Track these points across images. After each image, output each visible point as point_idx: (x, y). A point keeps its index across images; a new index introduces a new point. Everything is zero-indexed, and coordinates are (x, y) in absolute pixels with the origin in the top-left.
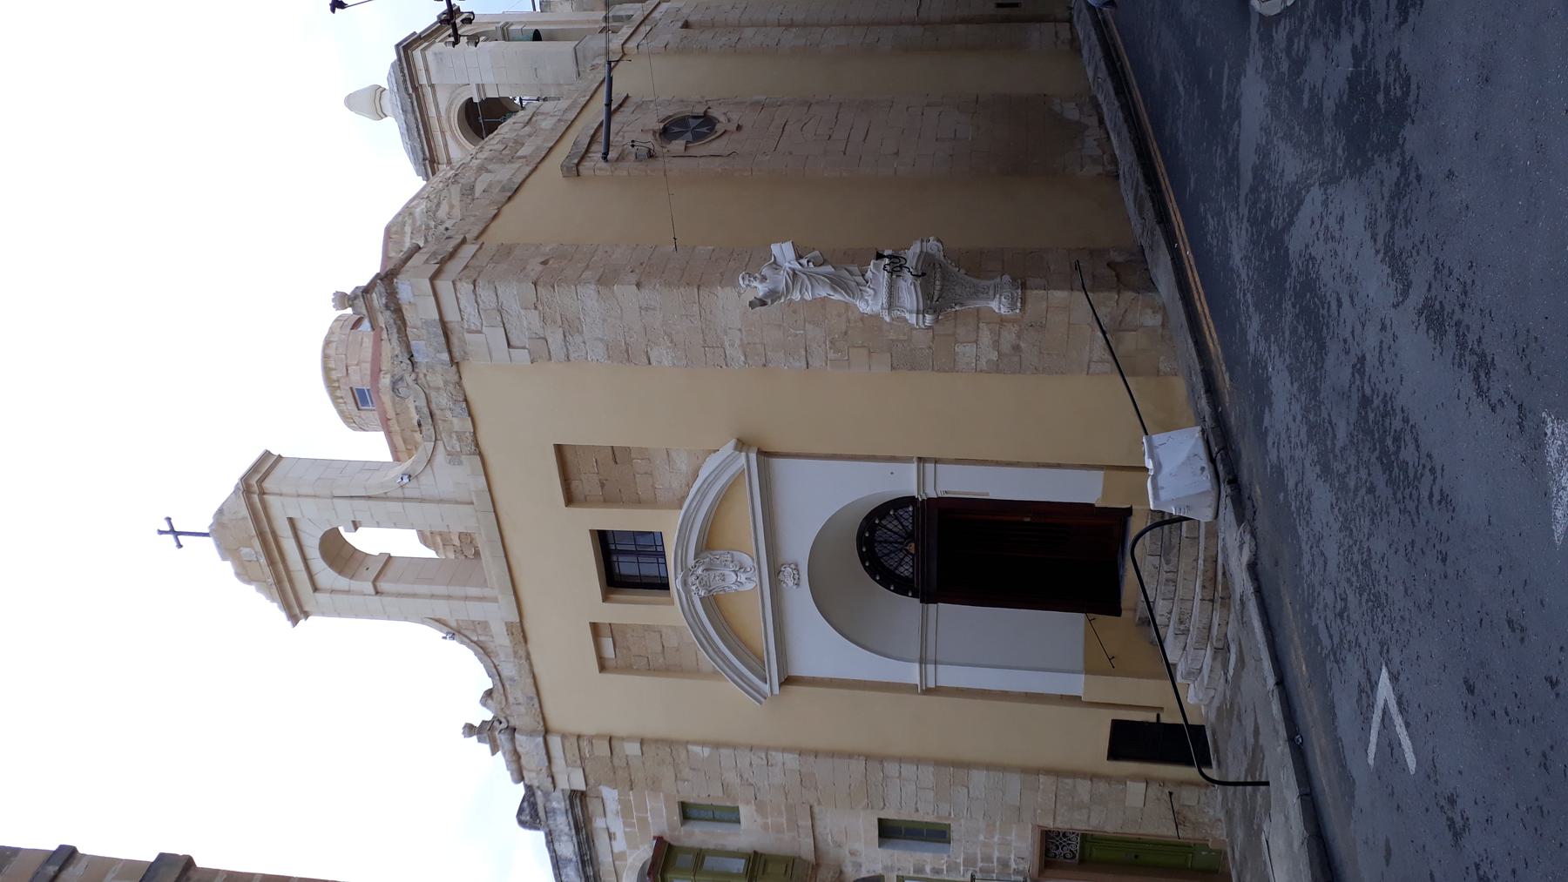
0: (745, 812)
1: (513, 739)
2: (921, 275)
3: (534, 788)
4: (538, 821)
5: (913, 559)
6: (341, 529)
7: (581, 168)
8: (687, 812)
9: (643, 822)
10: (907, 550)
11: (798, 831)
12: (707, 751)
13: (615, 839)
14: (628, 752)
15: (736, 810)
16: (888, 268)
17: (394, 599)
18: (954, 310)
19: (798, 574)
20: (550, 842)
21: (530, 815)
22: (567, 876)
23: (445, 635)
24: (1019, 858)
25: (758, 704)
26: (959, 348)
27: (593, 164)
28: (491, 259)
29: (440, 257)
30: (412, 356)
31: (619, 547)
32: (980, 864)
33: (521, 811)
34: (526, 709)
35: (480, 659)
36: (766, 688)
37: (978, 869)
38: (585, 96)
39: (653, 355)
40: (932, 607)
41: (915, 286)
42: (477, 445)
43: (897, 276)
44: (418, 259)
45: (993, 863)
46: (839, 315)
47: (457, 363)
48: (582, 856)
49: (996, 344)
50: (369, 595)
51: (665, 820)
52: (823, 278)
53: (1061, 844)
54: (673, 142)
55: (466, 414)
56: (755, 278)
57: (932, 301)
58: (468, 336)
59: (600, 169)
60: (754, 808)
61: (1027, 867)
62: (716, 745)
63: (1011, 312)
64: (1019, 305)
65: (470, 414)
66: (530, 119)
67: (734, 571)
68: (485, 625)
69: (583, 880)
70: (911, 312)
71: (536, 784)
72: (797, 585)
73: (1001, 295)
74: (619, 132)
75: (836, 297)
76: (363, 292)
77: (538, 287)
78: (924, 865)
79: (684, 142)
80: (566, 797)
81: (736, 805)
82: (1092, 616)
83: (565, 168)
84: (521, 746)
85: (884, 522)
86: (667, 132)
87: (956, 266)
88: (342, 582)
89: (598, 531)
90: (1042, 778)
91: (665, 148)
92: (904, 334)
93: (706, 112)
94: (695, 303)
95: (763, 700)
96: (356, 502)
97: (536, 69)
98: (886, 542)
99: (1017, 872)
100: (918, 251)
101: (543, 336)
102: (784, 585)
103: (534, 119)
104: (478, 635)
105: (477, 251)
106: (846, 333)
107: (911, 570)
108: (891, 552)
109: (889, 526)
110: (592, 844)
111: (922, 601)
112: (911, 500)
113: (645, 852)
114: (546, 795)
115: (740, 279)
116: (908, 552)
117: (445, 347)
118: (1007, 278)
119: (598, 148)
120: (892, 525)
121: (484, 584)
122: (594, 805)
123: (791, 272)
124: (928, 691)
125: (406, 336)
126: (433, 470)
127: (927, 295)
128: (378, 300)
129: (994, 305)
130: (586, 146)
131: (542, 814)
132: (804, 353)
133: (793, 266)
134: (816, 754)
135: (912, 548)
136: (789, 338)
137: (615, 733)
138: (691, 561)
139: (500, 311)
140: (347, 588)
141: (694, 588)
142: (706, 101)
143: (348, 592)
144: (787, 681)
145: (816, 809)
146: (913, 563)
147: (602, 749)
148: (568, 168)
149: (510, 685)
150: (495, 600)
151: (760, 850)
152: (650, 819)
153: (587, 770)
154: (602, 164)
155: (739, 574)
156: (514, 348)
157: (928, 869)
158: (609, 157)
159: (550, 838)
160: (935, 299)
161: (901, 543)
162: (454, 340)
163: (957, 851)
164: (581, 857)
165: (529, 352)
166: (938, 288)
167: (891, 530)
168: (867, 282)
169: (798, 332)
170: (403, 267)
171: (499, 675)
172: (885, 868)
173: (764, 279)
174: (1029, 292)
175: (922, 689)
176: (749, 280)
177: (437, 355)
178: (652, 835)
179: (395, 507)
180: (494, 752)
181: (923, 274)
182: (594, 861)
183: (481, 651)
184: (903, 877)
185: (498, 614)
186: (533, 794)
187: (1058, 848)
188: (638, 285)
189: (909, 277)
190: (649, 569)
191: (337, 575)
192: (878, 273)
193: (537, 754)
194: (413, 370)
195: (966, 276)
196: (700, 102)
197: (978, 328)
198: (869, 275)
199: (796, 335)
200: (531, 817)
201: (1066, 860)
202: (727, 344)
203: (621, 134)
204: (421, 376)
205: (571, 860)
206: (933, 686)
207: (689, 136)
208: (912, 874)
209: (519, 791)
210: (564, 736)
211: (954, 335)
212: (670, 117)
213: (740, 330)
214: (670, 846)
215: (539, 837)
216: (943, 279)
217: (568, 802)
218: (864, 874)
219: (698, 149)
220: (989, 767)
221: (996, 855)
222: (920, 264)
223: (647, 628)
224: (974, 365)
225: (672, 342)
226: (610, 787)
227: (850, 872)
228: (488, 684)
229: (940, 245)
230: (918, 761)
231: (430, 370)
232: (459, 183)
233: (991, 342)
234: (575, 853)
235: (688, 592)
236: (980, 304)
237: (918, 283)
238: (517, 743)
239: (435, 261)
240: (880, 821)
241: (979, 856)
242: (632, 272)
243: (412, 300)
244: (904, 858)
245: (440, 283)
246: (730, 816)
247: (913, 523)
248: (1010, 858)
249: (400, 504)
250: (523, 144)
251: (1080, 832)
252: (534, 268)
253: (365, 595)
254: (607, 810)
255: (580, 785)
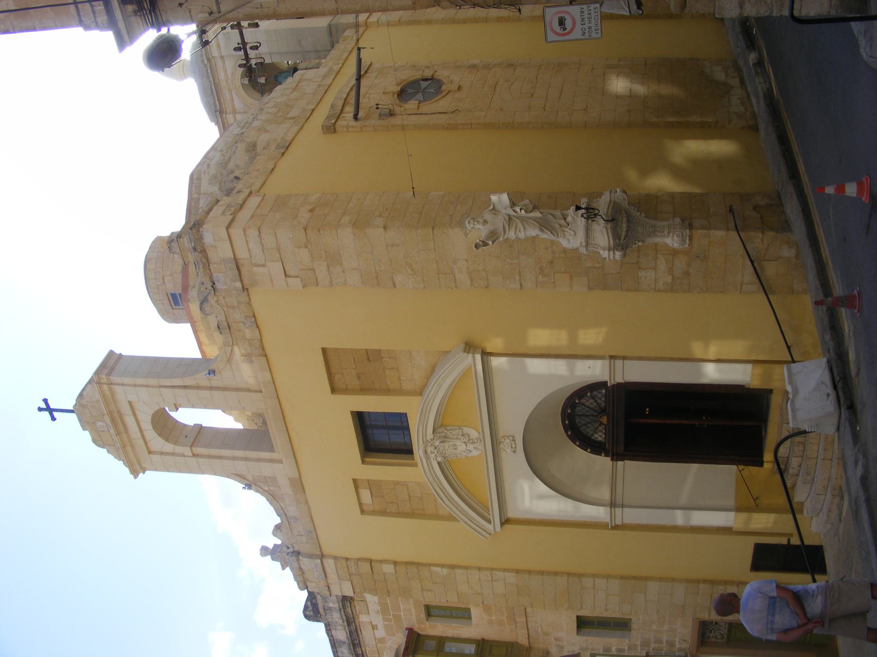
0: (474, 612)
1: (298, 560)
2: (612, 220)
3: (315, 593)
4: (319, 615)
5: (605, 428)
6: (167, 408)
7: (337, 126)
8: (430, 611)
9: (397, 618)
10: (600, 422)
11: (516, 625)
12: (445, 571)
13: (377, 629)
14: (385, 571)
15: (468, 610)
16: (585, 215)
17: (206, 460)
18: (637, 245)
19: (515, 444)
20: (329, 630)
21: (312, 611)
22: (342, 653)
23: (244, 486)
24: (682, 640)
25: (485, 539)
26: (642, 274)
27: (346, 122)
28: (271, 209)
29: (233, 209)
30: (214, 284)
31: (373, 423)
32: (653, 645)
33: (306, 608)
34: (307, 539)
35: (271, 503)
36: (490, 527)
37: (651, 649)
38: (338, 64)
39: (398, 279)
40: (620, 464)
41: (606, 229)
42: (263, 349)
43: (592, 221)
44: (217, 210)
45: (663, 644)
46: (546, 248)
47: (247, 289)
48: (352, 641)
49: (670, 271)
50: (188, 456)
51: (414, 617)
52: (532, 221)
53: (713, 629)
54: (409, 102)
55: (255, 326)
56: (478, 222)
57: (620, 240)
58: (256, 269)
59: (353, 127)
60: (482, 609)
61: (688, 646)
62: (453, 567)
63: (681, 247)
64: (688, 241)
65: (257, 327)
66: (297, 85)
67: (465, 442)
68: (274, 479)
69: (354, 655)
70: (604, 249)
71: (316, 591)
72: (514, 452)
73: (673, 234)
74: (366, 94)
75: (544, 236)
76: (177, 238)
77: (307, 231)
78: (611, 647)
79: (417, 102)
80: (340, 600)
81: (469, 607)
82: (741, 467)
83: (325, 128)
84: (304, 565)
85: (583, 401)
86: (403, 94)
87: (638, 211)
88: (169, 447)
89: (357, 412)
90: (702, 586)
91: (403, 107)
92: (599, 263)
93: (433, 75)
94: (430, 241)
95: (488, 536)
96: (176, 391)
97: (300, 41)
98: (584, 415)
99: (680, 649)
100: (608, 199)
101: (311, 267)
102: (504, 452)
103: (300, 84)
104: (268, 486)
105: (261, 202)
106: (552, 262)
107: (604, 436)
108: (589, 423)
109: (587, 404)
110: (359, 632)
111: (612, 460)
112: (603, 385)
113: (399, 639)
114: (325, 599)
115: (467, 223)
116: (601, 424)
117: (238, 277)
118: (678, 220)
119: (350, 109)
120: (589, 402)
121: (272, 450)
122: (358, 607)
123: (507, 218)
124: (616, 527)
125: (210, 270)
126: (231, 366)
127: (616, 236)
128: (186, 243)
129: (668, 241)
130: (340, 108)
131: (321, 611)
132: (518, 278)
133: (508, 213)
134: (530, 572)
135: (604, 420)
136: (506, 266)
137: (373, 558)
138: (430, 435)
139: (279, 250)
140: (172, 451)
141: (433, 455)
142: (433, 66)
143: (173, 454)
144: (505, 521)
145: (529, 610)
146: (606, 431)
147: (365, 568)
148: (327, 126)
149: (294, 522)
150: (280, 462)
151: (486, 638)
152: (403, 616)
153: (354, 583)
154: (353, 123)
155: (468, 444)
156: (290, 277)
157: (614, 649)
158: (359, 116)
159: (328, 628)
160: (623, 238)
161: (596, 416)
162: (244, 271)
163: (636, 636)
164: (352, 641)
165: (302, 280)
166: (625, 229)
167: (588, 407)
168: (568, 225)
169: (513, 262)
170: (206, 217)
171: (285, 515)
172: (582, 649)
173: (485, 222)
174: (695, 232)
175: (612, 526)
176: (474, 224)
177: (233, 284)
178: (405, 626)
179: (206, 393)
180: (283, 568)
181: (613, 220)
182: (362, 644)
183: (271, 497)
184: (595, 654)
185: (282, 472)
186: (315, 598)
187: (711, 632)
188: (385, 228)
189: (602, 222)
190: (396, 438)
191: (164, 441)
192: (579, 221)
193: (317, 571)
194: (215, 294)
195: (646, 219)
196: (428, 67)
197: (656, 258)
198: (569, 219)
199: (512, 264)
200: (314, 613)
201: (717, 640)
202: (456, 271)
203: (367, 96)
204: (221, 298)
205: (344, 643)
206: (621, 524)
207: (420, 96)
208: (601, 652)
209: (305, 594)
210: (336, 558)
211: (638, 263)
212: (405, 80)
213: (466, 260)
214: (418, 634)
215: (320, 627)
216: (628, 221)
217: (341, 604)
218: (565, 653)
219: (427, 107)
220: (661, 579)
221: (665, 638)
222: (610, 211)
223: (396, 483)
224: (653, 286)
225: (412, 270)
226: (372, 594)
227: (554, 650)
228: (278, 520)
229: (625, 195)
230: (608, 577)
231: (228, 294)
232: (245, 141)
233: (666, 269)
234: (347, 638)
235: (428, 458)
236: (657, 240)
237: (609, 226)
238: (301, 562)
239: (230, 213)
240: (578, 617)
241: (652, 640)
242: (380, 216)
243: (213, 243)
244: (597, 642)
245: (232, 231)
246: (463, 614)
247: (605, 401)
248: (675, 641)
249: (209, 391)
250: (292, 107)
251: (728, 621)
252: (304, 215)
253: (185, 456)
254: (370, 610)
255: (349, 593)
